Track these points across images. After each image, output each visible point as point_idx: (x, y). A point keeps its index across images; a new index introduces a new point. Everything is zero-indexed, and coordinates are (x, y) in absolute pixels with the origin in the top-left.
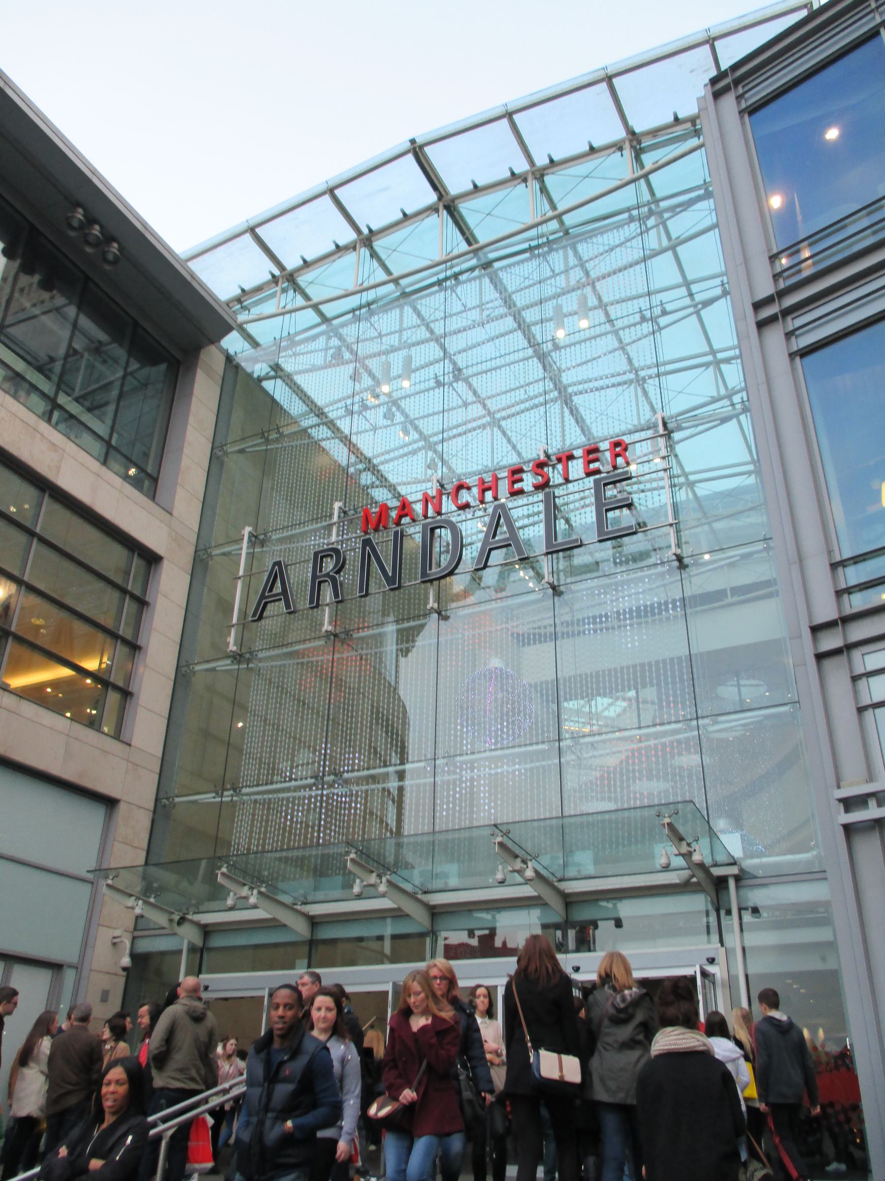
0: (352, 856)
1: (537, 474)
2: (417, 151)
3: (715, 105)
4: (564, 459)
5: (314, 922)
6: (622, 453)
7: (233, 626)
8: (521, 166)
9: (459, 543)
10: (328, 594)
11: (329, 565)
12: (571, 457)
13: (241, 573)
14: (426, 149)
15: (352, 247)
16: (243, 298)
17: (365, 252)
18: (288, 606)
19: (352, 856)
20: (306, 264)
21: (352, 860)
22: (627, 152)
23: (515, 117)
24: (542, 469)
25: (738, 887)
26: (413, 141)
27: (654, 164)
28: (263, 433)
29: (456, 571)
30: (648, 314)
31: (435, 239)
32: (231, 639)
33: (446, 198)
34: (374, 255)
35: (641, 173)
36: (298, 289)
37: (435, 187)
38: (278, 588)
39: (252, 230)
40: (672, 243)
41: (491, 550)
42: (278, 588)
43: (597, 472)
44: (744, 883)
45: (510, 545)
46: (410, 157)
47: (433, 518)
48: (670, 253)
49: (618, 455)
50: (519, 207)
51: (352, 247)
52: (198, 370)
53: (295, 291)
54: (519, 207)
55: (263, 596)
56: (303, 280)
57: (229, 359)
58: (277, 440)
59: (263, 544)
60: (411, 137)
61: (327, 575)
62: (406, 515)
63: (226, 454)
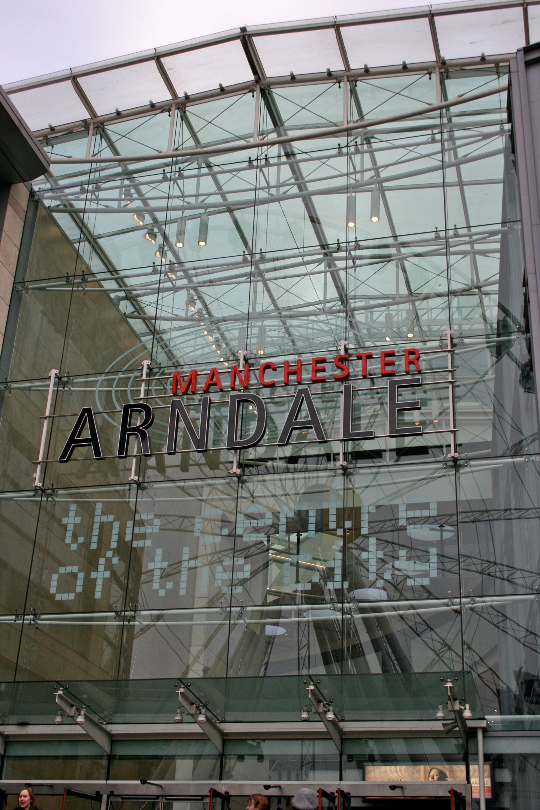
0: (60, 692)
1: (338, 367)
2: (246, 38)
3: (526, 73)
4: (364, 357)
5: (114, 739)
6: (415, 361)
7: (39, 463)
8: (338, 66)
9: (264, 418)
10: (134, 445)
11: (138, 421)
12: (370, 356)
13: (47, 414)
14: (255, 39)
15: (164, 108)
16: (52, 135)
17: (177, 114)
18: (97, 453)
19: (60, 692)
20: (119, 115)
21: (59, 695)
22: (435, 77)
23: (342, 30)
24: (342, 363)
25: (484, 737)
26: (243, 29)
27: (459, 96)
28: (68, 277)
29: (260, 443)
30: (442, 234)
31: (244, 116)
32: (37, 475)
33: (263, 82)
34: (184, 118)
35: (444, 103)
36: (104, 135)
37: (255, 71)
38: (86, 434)
39: (74, 78)
40: (457, 161)
41: (293, 429)
42: (86, 434)
43: (393, 374)
44: (489, 734)
45: (311, 427)
46: (238, 43)
47: (240, 390)
48: (465, 187)
49: (411, 363)
50: (331, 105)
51: (164, 108)
52: (8, 205)
53: (101, 137)
54: (331, 105)
55: (71, 440)
56: (112, 129)
57: (32, 193)
58: (79, 284)
59: (65, 384)
60: (242, 25)
61: (137, 429)
62: (215, 384)
63: (27, 289)
